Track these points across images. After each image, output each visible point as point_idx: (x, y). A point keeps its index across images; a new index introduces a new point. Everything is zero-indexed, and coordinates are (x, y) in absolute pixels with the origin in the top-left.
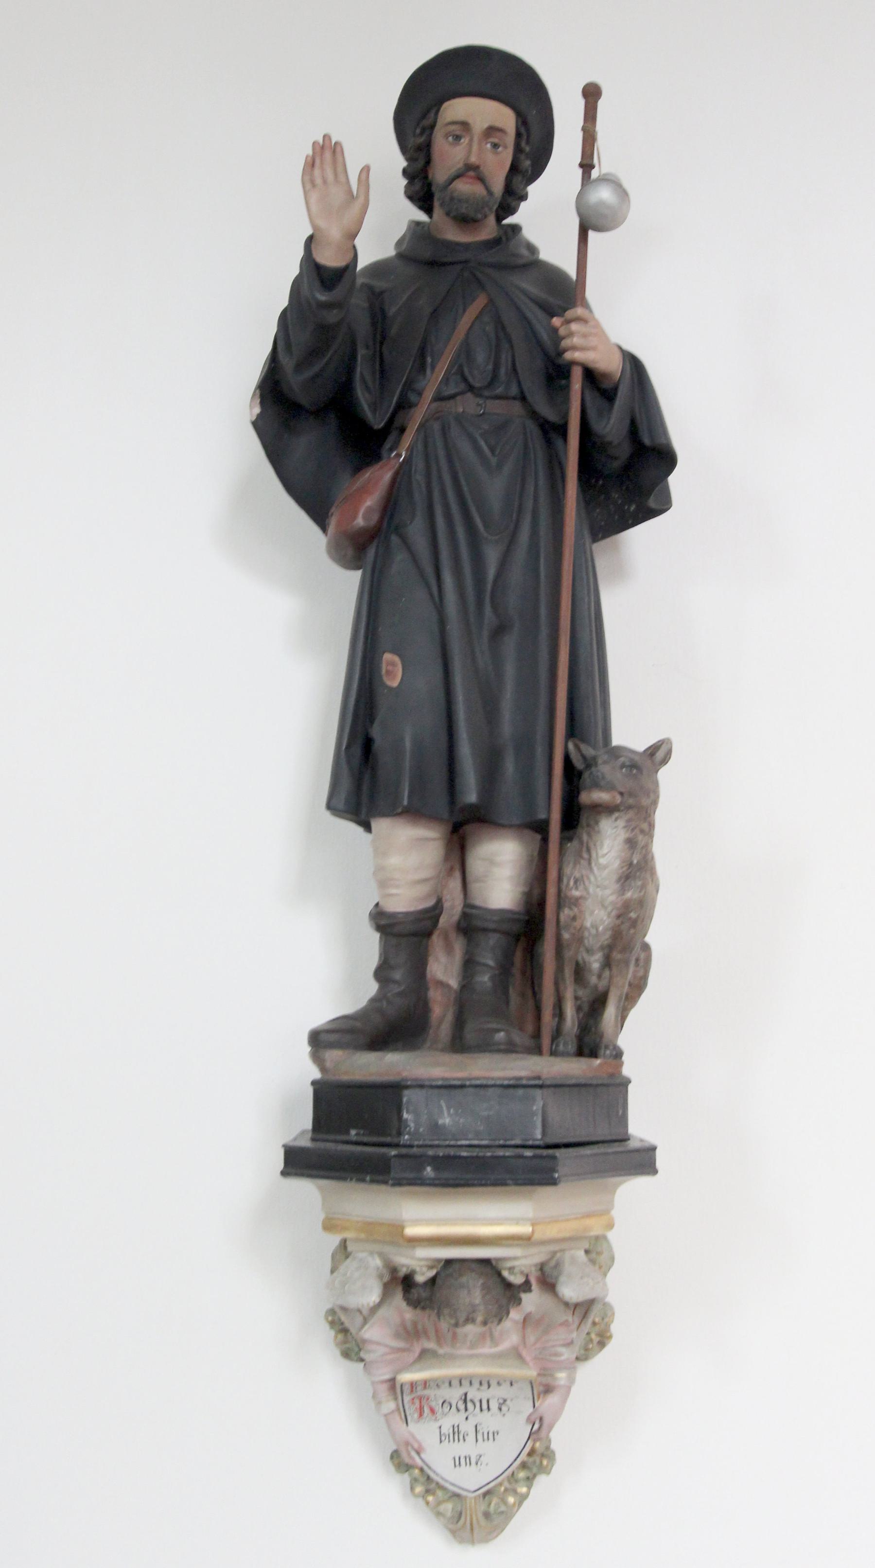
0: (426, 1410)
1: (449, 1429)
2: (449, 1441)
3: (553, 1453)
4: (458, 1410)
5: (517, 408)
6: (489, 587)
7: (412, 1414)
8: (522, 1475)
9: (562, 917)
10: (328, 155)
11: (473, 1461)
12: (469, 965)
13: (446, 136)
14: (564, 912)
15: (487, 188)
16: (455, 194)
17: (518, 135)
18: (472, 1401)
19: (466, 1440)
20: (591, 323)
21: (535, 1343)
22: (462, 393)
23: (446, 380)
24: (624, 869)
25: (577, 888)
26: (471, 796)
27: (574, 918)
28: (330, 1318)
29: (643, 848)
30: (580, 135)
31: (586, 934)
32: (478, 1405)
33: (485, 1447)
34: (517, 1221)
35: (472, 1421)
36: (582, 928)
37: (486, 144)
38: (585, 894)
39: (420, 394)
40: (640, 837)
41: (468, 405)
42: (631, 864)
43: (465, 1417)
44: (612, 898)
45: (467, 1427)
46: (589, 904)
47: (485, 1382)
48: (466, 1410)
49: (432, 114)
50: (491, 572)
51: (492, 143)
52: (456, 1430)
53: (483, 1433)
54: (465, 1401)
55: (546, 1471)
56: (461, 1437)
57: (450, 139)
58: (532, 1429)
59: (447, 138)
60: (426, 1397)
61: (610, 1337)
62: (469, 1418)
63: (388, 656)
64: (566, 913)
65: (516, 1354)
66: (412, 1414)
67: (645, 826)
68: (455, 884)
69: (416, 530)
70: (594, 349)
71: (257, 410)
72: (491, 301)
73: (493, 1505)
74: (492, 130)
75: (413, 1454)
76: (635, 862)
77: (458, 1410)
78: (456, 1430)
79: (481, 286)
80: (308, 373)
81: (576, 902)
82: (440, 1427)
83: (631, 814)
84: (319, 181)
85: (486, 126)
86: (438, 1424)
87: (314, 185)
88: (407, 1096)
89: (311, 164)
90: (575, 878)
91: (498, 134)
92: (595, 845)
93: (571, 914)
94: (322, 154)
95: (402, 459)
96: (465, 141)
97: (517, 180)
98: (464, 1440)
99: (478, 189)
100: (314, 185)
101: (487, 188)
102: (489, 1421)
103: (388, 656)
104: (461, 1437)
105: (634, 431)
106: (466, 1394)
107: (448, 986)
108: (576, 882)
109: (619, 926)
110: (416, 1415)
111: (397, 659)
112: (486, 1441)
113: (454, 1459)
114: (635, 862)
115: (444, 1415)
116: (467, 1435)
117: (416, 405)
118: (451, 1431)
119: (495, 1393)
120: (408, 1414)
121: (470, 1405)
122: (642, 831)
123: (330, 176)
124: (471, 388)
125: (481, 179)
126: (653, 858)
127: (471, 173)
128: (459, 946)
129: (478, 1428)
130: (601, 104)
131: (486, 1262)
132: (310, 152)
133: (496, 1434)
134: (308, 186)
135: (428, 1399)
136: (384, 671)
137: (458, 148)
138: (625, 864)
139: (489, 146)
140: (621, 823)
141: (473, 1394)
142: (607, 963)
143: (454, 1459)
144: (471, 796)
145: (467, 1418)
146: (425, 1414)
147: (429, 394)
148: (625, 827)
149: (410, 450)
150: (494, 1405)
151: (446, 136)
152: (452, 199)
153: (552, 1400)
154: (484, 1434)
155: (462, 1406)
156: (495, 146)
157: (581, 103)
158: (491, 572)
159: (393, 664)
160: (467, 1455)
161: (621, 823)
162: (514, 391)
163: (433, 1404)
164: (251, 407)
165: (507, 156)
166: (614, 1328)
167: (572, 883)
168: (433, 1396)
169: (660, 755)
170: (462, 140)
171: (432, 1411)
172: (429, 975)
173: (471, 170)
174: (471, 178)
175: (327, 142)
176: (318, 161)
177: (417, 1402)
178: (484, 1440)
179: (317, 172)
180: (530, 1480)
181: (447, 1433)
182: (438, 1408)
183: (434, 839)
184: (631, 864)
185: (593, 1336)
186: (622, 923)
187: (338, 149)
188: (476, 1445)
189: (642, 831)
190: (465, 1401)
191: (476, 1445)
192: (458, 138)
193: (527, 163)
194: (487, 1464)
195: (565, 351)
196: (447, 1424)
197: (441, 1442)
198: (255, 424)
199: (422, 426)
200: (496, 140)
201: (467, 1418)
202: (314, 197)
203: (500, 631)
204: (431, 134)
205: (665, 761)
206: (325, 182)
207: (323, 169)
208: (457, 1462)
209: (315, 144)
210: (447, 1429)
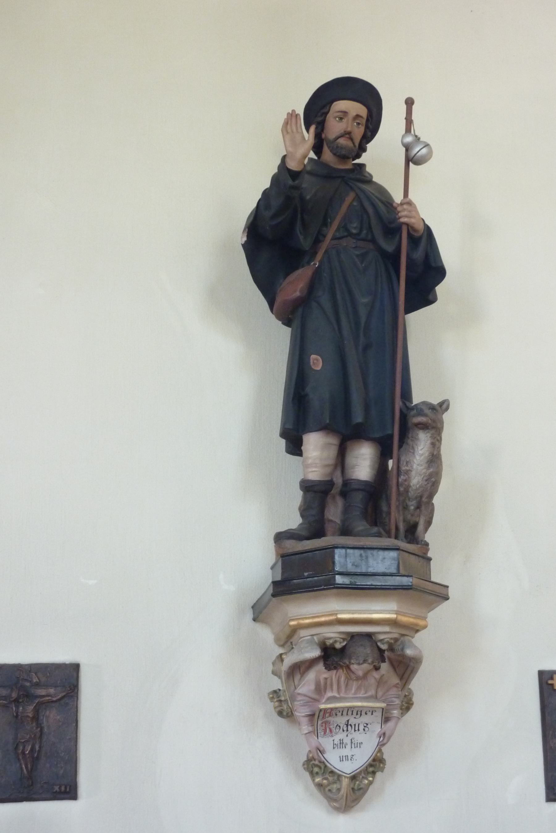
0: (328, 730)
1: (338, 742)
2: (338, 748)
3: (385, 760)
4: (343, 731)
5: (371, 246)
6: (363, 325)
7: (321, 733)
8: (371, 769)
9: (400, 480)
10: (294, 120)
11: (349, 758)
12: (346, 510)
13: (335, 118)
14: (401, 477)
15: (354, 143)
16: (339, 145)
17: (367, 120)
18: (351, 725)
19: (346, 748)
20: (413, 206)
21: (382, 696)
22: (346, 236)
23: (338, 229)
24: (430, 457)
25: (407, 466)
26: (358, 418)
27: (405, 480)
28: (271, 696)
29: (438, 448)
30: (404, 121)
31: (410, 490)
32: (353, 727)
33: (356, 751)
34: (389, 612)
35: (350, 737)
36: (409, 486)
37: (354, 122)
38: (411, 468)
39: (325, 236)
40: (437, 443)
41: (350, 242)
42: (433, 455)
43: (346, 735)
44: (424, 471)
45: (347, 740)
46: (413, 473)
47: (360, 712)
48: (347, 730)
49: (328, 108)
50: (363, 320)
51: (357, 123)
52: (341, 742)
53: (355, 744)
54: (347, 725)
55: (382, 770)
56: (344, 747)
57: (337, 119)
58: (379, 740)
59: (336, 119)
60: (329, 722)
61: (412, 704)
62: (348, 735)
63: (313, 357)
64: (402, 478)
65: (375, 698)
66: (321, 733)
67: (439, 438)
68: (338, 473)
69: (325, 300)
70: (414, 217)
71: (245, 239)
72: (357, 195)
73: (356, 785)
74: (358, 116)
75: (320, 754)
76: (435, 454)
77: (343, 731)
78: (341, 742)
79: (352, 189)
80: (274, 222)
81: (408, 472)
82: (334, 740)
83: (433, 431)
84: (289, 130)
85: (355, 114)
86: (333, 738)
87: (288, 133)
88: (337, 551)
89: (286, 123)
90: (406, 461)
91: (360, 118)
92: (416, 445)
93: (404, 478)
94: (291, 119)
95: (317, 266)
96: (345, 121)
97: (364, 141)
98: (345, 747)
99: (350, 144)
100: (288, 133)
101: (354, 143)
102: (359, 737)
103: (313, 357)
104: (344, 747)
105: (427, 257)
106: (348, 721)
107: (335, 522)
108: (407, 463)
109: (426, 485)
110: (322, 733)
111: (319, 358)
112: (356, 748)
113: (340, 757)
114: (435, 454)
115: (336, 733)
116: (347, 745)
117: (323, 241)
118: (339, 742)
119: (365, 719)
120: (319, 732)
121: (349, 727)
122: (438, 440)
123: (295, 130)
124: (350, 235)
125: (351, 139)
126: (441, 455)
127: (347, 136)
128: (340, 502)
129: (353, 740)
130: (414, 107)
131: (369, 636)
132: (286, 117)
133: (361, 744)
134: (285, 133)
135: (329, 724)
136: (312, 363)
137: (341, 124)
138: (431, 454)
139: (355, 124)
140: (429, 435)
141: (352, 721)
142: (418, 507)
143: (340, 757)
144: (358, 418)
145: (347, 736)
146: (327, 733)
147: (329, 236)
148: (430, 437)
149: (321, 262)
150: (361, 728)
151: (335, 118)
152: (337, 147)
153: (390, 724)
154: (345, 760)
155: (345, 729)
156: (358, 124)
157: (405, 107)
158: (363, 320)
159: (317, 360)
160: (342, 761)
161: (429, 435)
162: (370, 237)
163: (331, 727)
164: (242, 238)
165: (362, 129)
166: (414, 699)
167: (405, 464)
168: (332, 722)
169: (444, 406)
170: (343, 120)
171: (331, 731)
172: (325, 517)
173: (348, 134)
174: (347, 138)
175: (294, 114)
176: (289, 122)
177: (324, 725)
178: (355, 748)
179: (289, 127)
180: (374, 773)
181: (337, 744)
182: (334, 730)
183: (335, 445)
184: (433, 455)
185: (404, 703)
186: (428, 483)
187: (298, 117)
188: (351, 750)
189: (438, 440)
190: (347, 725)
191: (351, 750)
192: (341, 119)
193: (369, 134)
194: (356, 760)
195: (399, 218)
196: (337, 738)
197: (334, 748)
198: (243, 245)
199: (326, 252)
200: (358, 121)
201: (347, 736)
202: (288, 137)
203: (366, 348)
204: (326, 117)
205: (447, 409)
206: (292, 132)
207: (291, 125)
208: (341, 760)
209: (288, 114)
210: (337, 741)
